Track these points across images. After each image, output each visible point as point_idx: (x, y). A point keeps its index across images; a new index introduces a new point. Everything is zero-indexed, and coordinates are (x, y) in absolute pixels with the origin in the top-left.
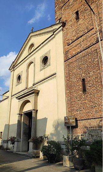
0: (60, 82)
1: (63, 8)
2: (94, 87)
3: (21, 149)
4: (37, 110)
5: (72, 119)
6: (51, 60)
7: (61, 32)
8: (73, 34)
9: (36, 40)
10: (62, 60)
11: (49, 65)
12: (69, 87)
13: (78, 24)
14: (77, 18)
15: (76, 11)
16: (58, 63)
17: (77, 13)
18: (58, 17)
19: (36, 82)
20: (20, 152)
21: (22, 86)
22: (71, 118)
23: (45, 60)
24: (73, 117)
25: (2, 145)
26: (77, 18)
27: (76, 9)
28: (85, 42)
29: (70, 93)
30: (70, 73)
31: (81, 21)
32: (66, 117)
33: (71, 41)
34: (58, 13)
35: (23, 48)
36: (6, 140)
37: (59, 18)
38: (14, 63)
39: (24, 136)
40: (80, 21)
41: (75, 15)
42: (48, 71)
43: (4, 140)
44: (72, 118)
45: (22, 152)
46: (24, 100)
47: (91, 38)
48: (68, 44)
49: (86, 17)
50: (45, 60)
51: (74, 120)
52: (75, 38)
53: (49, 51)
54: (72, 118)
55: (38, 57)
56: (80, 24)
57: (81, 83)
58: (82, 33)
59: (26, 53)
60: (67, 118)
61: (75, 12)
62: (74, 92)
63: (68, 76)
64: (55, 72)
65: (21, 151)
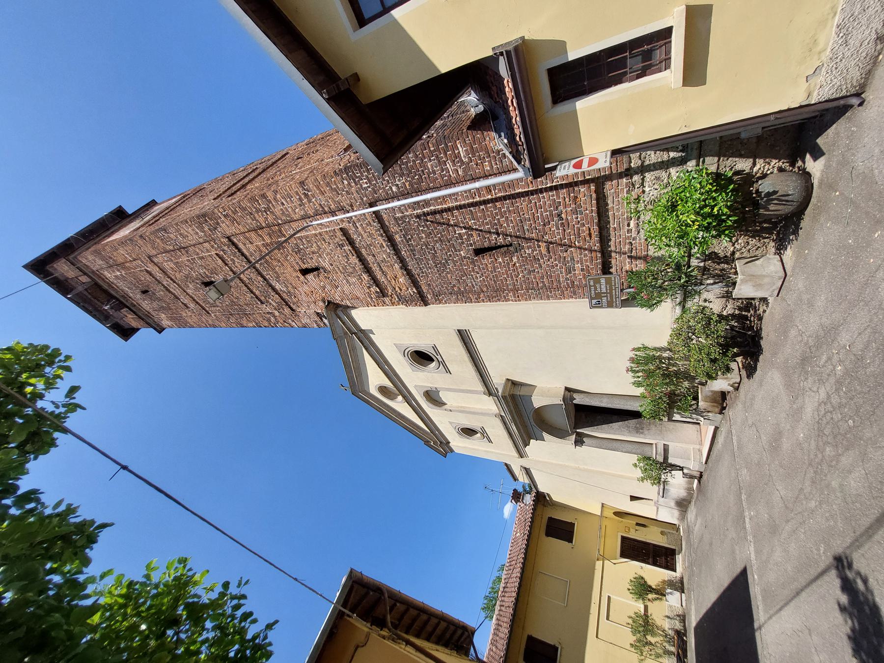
0: (483, 318)
1: (294, 307)
2: (499, 222)
3: (691, 447)
4: (567, 389)
5: (598, 286)
7: (354, 313)
8: (354, 284)
10: (418, 311)
11: (435, 348)
12: (496, 292)
14: (346, 150)
15: (300, 275)
17: (305, 272)
19: (480, 387)
20: (700, 451)
21: (497, 430)
22: (596, 289)
23: (422, 358)
24: (592, 283)
25: (673, 504)
26: (346, 150)
27: (295, 274)
28: (375, 251)
31: (325, 263)
32: (591, 302)
33: (374, 289)
34: (305, 320)
39: (646, 432)
41: (310, 277)
44: (594, 286)
46: (533, 423)
47: (365, 235)
48: (382, 294)
49: (315, 248)
50: (422, 358)
52: (365, 276)
53: (744, 573)
54: (594, 286)
55: (416, 380)
57: (486, 260)
58: (354, 260)
60: (594, 301)
61: (302, 278)
62: (512, 277)
63: (464, 295)
65: (698, 447)
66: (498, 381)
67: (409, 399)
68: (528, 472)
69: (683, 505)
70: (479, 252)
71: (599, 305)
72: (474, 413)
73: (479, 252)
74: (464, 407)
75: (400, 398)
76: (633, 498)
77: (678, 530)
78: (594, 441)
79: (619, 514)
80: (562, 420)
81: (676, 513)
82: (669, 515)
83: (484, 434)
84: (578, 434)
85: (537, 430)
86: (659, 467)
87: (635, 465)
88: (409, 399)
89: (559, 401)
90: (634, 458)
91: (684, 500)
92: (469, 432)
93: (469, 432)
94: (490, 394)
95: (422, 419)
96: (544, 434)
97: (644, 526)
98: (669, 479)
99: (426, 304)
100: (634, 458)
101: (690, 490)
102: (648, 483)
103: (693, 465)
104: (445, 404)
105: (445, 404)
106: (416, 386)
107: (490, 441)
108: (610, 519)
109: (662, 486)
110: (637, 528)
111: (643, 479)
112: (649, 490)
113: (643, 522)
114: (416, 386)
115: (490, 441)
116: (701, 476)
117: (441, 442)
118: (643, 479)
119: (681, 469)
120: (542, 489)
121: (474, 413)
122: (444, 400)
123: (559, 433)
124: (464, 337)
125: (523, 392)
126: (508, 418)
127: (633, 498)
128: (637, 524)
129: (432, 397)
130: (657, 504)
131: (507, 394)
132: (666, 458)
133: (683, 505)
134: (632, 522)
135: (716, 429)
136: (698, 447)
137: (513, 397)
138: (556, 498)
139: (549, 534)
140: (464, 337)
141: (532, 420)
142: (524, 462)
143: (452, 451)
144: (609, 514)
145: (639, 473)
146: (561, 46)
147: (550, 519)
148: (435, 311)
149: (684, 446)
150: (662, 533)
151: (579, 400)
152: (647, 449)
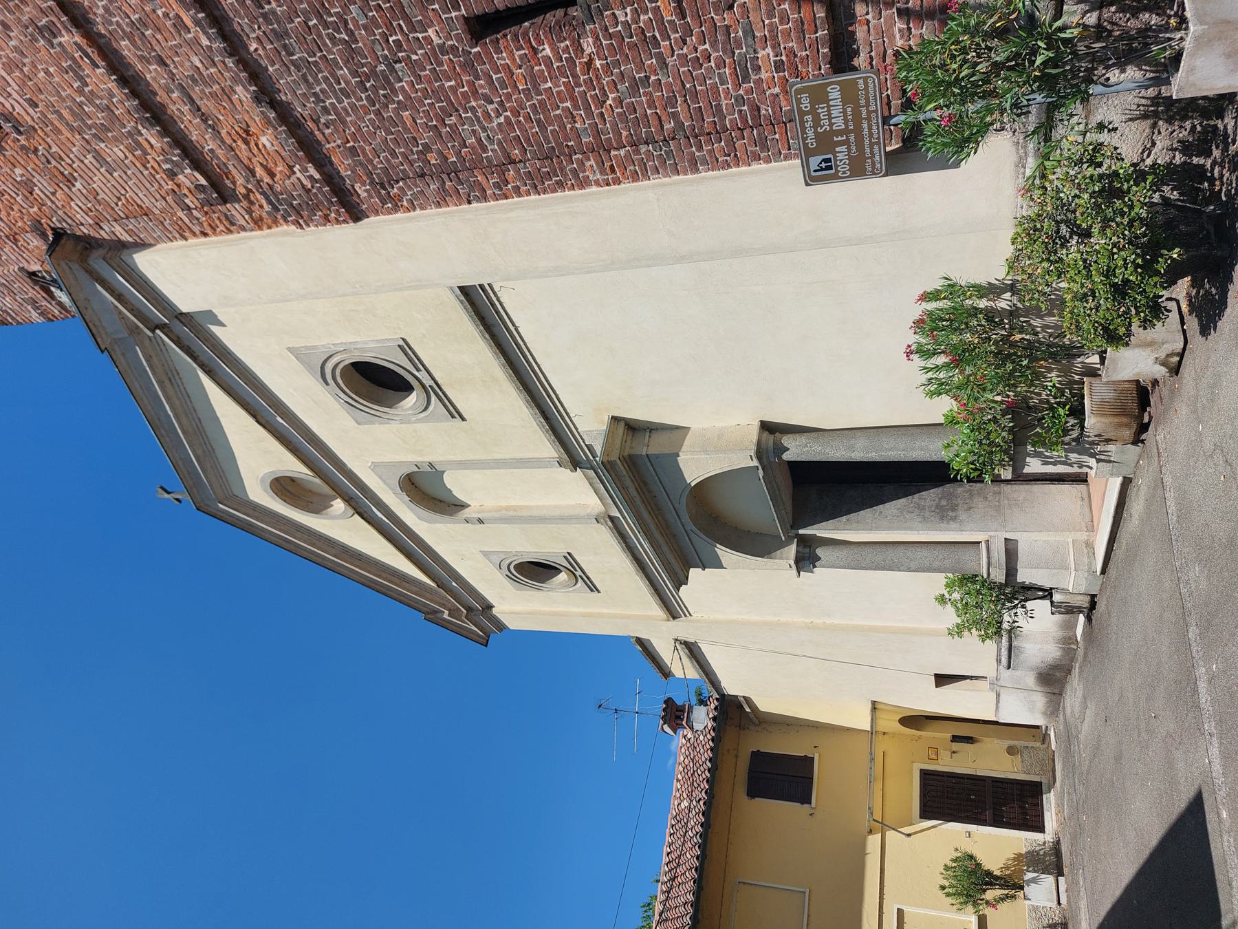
0: (526, 241)
3: (1069, 538)
4: (766, 427)
5: (822, 112)
6: (373, 341)
7: (144, 261)
9: (257, 459)
10: (339, 238)
12: (548, 163)
13: (28, 116)
16: (384, 275)
18: (33, 302)
19: (547, 449)
20: (1089, 545)
21: (605, 557)
22: (817, 122)
23: (376, 382)
25: (1030, 680)
29: (601, 149)
30: (433, 159)
32: (806, 166)
35: (874, 128)
36: (992, 290)
37: (34, 292)
38: (436, 612)
40: (1192, 28)
42: (456, 355)
43: (999, 661)
45: (1092, 528)
46: (690, 526)
48: (219, 197)
50: (376, 382)
51: (834, 94)
52: (151, 137)
54: (813, 112)
56: (34, 105)
59: (340, 525)
60: (815, 161)
62: (588, 108)
63: (461, 177)
64: (449, 293)
65: (1084, 536)
66: (590, 426)
68: (692, 650)
69: (1053, 679)
72: (541, 520)
74: (515, 508)
76: (942, 680)
77: (1045, 738)
79: (914, 721)
80: (759, 509)
81: (1040, 700)
82: (1022, 706)
84: (805, 542)
85: (701, 541)
86: (996, 596)
87: (942, 600)
89: (745, 459)
96: (724, 553)
97: (969, 740)
99: (356, 214)
100: (937, 583)
101: (1068, 642)
102: (972, 638)
103: (1073, 582)
104: (463, 506)
106: (375, 467)
107: (593, 588)
108: (894, 735)
110: (956, 746)
111: (959, 631)
112: (977, 654)
113: (965, 732)
114: (375, 467)
115: (593, 588)
116: (1093, 605)
118: (959, 631)
120: (732, 688)
121: (541, 520)
125: (655, 446)
127: (942, 680)
128: (955, 739)
129: (425, 489)
132: (1011, 571)
133: (1053, 679)
134: (941, 735)
135: (1127, 483)
136: (1084, 536)
138: (765, 704)
139: (753, 793)
140: (480, 304)
141: (686, 518)
142: (682, 629)
144: (890, 723)
145: (950, 617)
147: (757, 756)
148: (386, 233)
150: (1011, 751)
151: (796, 450)
152: (967, 555)
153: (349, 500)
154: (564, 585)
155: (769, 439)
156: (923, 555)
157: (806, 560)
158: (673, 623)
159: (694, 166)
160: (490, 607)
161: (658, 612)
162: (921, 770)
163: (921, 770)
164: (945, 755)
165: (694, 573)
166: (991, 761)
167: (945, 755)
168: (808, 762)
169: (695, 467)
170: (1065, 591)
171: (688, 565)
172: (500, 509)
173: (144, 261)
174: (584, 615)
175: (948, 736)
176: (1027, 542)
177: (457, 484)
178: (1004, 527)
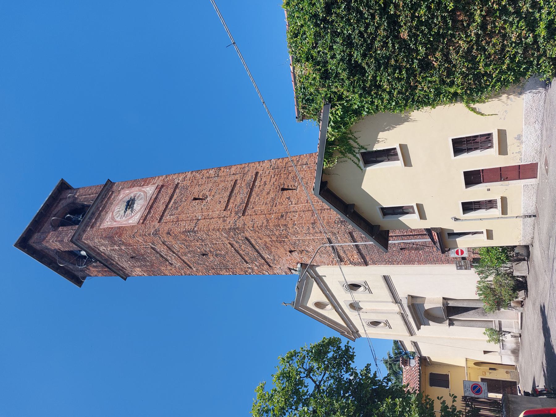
4: (444, 298)
7: (317, 269)
21: (397, 323)
25: (509, 353)
38: (343, 332)
65: (516, 320)
66: (402, 294)
67: (337, 307)
68: (415, 344)
69: (515, 352)
70: (401, 249)
71: (461, 269)
72: (383, 313)
73: (401, 249)
74: (376, 310)
75: (330, 307)
76: (485, 352)
77: (516, 369)
78: (460, 323)
79: (478, 364)
80: (442, 314)
81: (513, 358)
82: (508, 360)
83: (387, 324)
84: (450, 319)
85: (426, 320)
86: (497, 334)
87: (485, 333)
88: (337, 307)
89: (440, 305)
90: (484, 330)
91: (515, 349)
92: (375, 323)
93: (375, 323)
94: (396, 302)
95: (343, 319)
96: (430, 322)
97: (494, 369)
98: (504, 339)
99: (366, 264)
100: (484, 330)
101: (517, 343)
102: (492, 343)
103: (516, 331)
104: (362, 309)
105: (362, 309)
106: (345, 301)
107: (390, 327)
108: (472, 368)
109: (501, 343)
110: (491, 371)
111: (489, 341)
112: (494, 347)
113: (493, 367)
114: (345, 301)
115: (390, 327)
116: (520, 336)
117: (352, 332)
118: (489, 341)
119: (510, 333)
120: (424, 354)
121: (383, 313)
122: (361, 306)
123: (438, 320)
124: (386, 279)
125: (418, 302)
126: (545, 365)
127: (485, 352)
128: (490, 369)
129: (354, 306)
130: (500, 354)
131: (410, 304)
132: (500, 328)
133: (515, 352)
134: (487, 368)
135: (522, 314)
136: (516, 320)
137: (413, 305)
138: (433, 359)
139: (431, 385)
140: (386, 279)
141: (423, 315)
142: (414, 339)
143: (360, 336)
144: (471, 365)
145: (487, 338)
146: (453, 230)
147: (431, 374)
148: (371, 269)
149: (509, 320)
150: (507, 372)
151: (451, 304)
152: (490, 324)
153: (334, 307)
154: (382, 327)
155: (445, 301)
156: (479, 323)
157: (451, 324)
158: (411, 337)
159: (435, 264)
160: (358, 331)
161: (407, 334)
162: (452, 140)
163: (452, 140)
164: (488, 374)
165: (422, 326)
166: (501, 375)
167: (488, 374)
168: (447, 376)
169: (427, 306)
170: (513, 333)
171: (421, 325)
172: (371, 310)
173: (317, 269)
174: (386, 334)
175: (488, 368)
176: (503, 322)
177: (361, 305)
178: (498, 318)
